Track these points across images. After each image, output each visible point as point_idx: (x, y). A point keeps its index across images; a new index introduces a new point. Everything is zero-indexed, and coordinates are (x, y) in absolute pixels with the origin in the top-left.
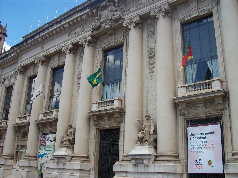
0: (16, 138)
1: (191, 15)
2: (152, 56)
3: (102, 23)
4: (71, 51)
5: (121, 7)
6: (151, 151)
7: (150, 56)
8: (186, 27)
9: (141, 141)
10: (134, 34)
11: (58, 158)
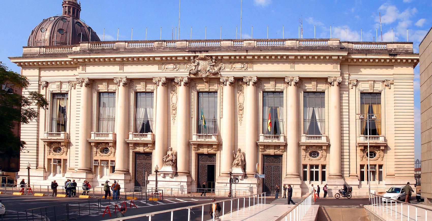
0: (129, 153)
3: (200, 71)
4: (231, 84)
7: (240, 109)
8: (364, 97)
9: (164, 162)
11: (164, 174)
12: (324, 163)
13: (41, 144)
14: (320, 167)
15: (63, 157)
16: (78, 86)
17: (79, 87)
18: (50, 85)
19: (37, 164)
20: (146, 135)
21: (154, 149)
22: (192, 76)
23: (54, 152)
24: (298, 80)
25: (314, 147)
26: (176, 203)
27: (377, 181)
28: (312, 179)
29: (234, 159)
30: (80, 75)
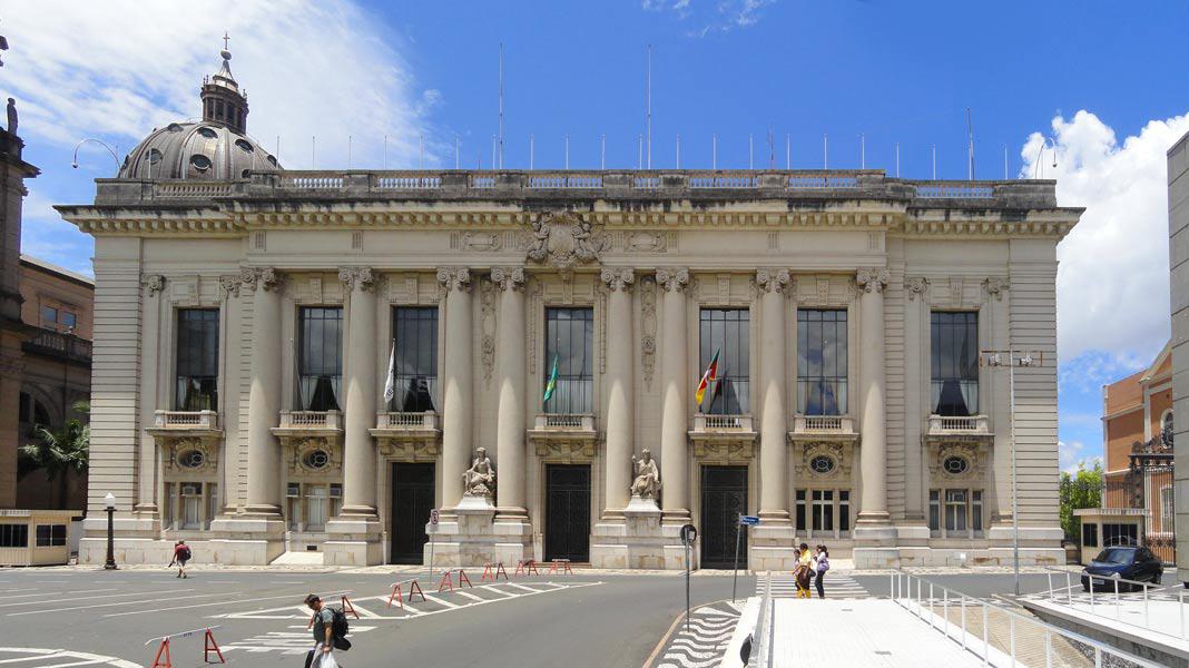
1: (718, 300)
2: (649, 349)
3: (551, 253)
4: (464, 285)
5: (594, 235)
6: (653, 508)
7: (648, 350)
9: (466, 487)
10: (618, 298)
11: (467, 515)
12: (845, 487)
13: (148, 444)
14: (836, 495)
15: (203, 480)
16: (245, 288)
17: (249, 292)
18: (170, 286)
19: (136, 499)
20: (421, 418)
21: (441, 453)
22: (532, 266)
23: (303, 465)
24: (686, 276)
25: (823, 446)
26: (539, 591)
27: (836, 530)
28: (816, 526)
29: (634, 476)
30: (250, 259)
